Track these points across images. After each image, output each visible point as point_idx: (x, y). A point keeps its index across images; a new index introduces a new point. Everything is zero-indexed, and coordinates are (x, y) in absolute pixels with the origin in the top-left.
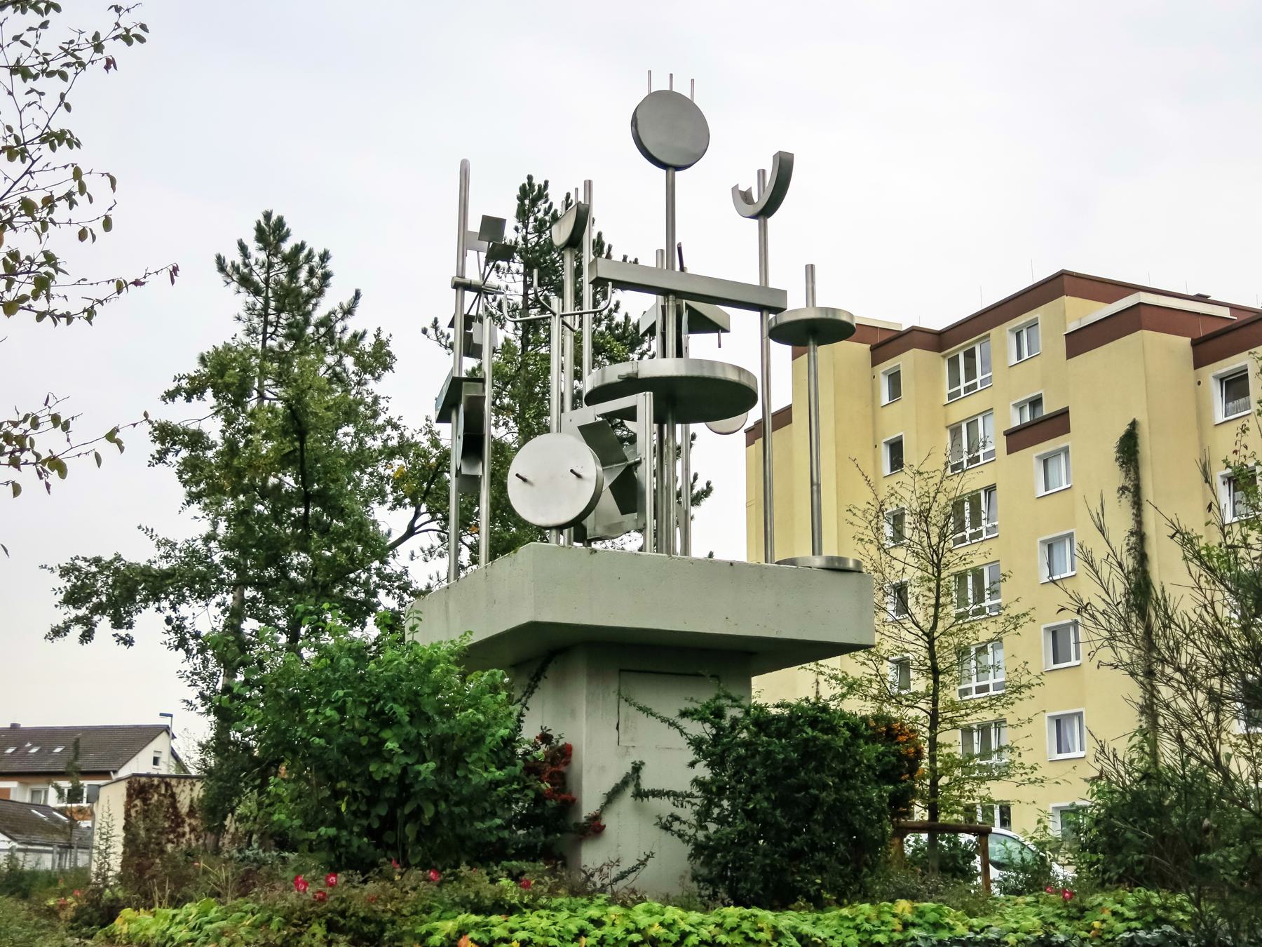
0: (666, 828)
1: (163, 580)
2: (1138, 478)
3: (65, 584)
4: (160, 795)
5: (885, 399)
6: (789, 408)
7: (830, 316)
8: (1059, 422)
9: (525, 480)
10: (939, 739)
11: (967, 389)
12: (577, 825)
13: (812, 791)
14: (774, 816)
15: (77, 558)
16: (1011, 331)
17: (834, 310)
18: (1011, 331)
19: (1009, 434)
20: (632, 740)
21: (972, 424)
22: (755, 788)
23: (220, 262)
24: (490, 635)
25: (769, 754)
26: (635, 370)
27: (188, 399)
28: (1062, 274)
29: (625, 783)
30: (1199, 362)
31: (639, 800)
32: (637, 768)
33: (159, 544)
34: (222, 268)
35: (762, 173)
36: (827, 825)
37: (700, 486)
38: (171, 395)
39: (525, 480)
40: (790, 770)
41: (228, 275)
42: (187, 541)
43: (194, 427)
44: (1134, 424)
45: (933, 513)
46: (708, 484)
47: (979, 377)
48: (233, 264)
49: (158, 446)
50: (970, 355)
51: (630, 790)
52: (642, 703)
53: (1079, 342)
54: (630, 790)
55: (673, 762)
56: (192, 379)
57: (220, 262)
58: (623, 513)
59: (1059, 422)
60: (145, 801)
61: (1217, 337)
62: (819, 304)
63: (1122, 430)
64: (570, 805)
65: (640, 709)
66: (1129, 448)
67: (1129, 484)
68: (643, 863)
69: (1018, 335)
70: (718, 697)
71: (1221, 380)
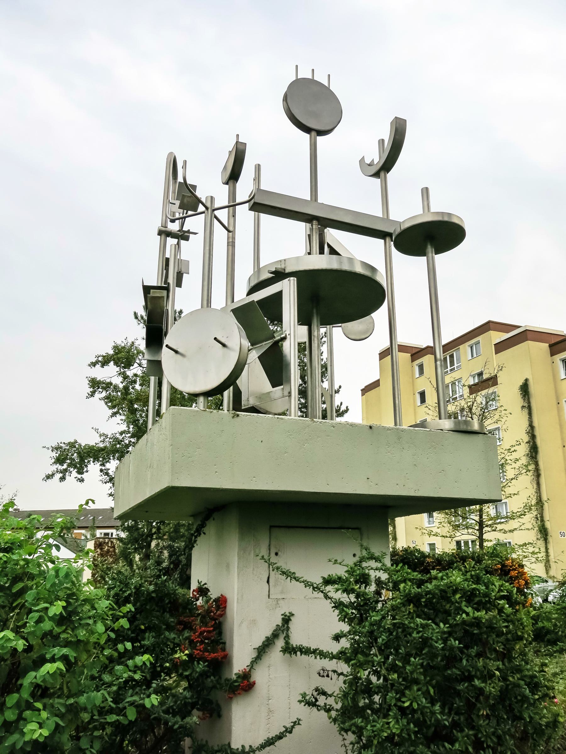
0: (312, 704)
1: (99, 452)
2: (529, 402)
3: (55, 454)
4: (108, 546)
5: (417, 375)
6: (379, 380)
7: (446, 219)
8: (493, 381)
9: (176, 352)
10: (485, 537)
11: (451, 370)
12: (227, 680)
13: (477, 682)
14: (433, 713)
15: (61, 443)
16: (469, 346)
17: (449, 215)
18: (469, 346)
19: (470, 387)
20: (282, 592)
21: (453, 383)
22: (411, 682)
23: (135, 314)
24: (153, 493)
25: (425, 642)
26: (283, 266)
27: (102, 366)
28: (489, 322)
29: (275, 635)
30: (552, 354)
31: (287, 655)
32: (287, 620)
33: (100, 436)
34: (136, 317)
35: (381, 142)
36: (493, 714)
37: (343, 408)
38: (94, 364)
39: (176, 352)
40: (452, 659)
41: (139, 321)
42: (112, 434)
43: (108, 381)
44: (526, 380)
45: (474, 408)
46: (347, 407)
47: (456, 365)
48: (141, 315)
49: (91, 390)
50: (452, 356)
51: (280, 643)
52: (285, 567)
53: (500, 347)
54: (280, 643)
55: (321, 624)
56: (104, 357)
57: (135, 314)
58: (273, 387)
59: (493, 381)
60: (101, 549)
61: (559, 344)
62: (432, 210)
63: (521, 382)
64: (221, 662)
65: (283, 573)
66: (525, 389)
67: (526, 405)
68: (289, 731)
69: (472, 348)
70: (362, 560)
71: (563, 361)
